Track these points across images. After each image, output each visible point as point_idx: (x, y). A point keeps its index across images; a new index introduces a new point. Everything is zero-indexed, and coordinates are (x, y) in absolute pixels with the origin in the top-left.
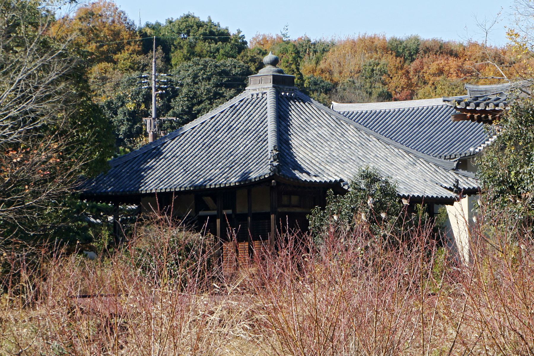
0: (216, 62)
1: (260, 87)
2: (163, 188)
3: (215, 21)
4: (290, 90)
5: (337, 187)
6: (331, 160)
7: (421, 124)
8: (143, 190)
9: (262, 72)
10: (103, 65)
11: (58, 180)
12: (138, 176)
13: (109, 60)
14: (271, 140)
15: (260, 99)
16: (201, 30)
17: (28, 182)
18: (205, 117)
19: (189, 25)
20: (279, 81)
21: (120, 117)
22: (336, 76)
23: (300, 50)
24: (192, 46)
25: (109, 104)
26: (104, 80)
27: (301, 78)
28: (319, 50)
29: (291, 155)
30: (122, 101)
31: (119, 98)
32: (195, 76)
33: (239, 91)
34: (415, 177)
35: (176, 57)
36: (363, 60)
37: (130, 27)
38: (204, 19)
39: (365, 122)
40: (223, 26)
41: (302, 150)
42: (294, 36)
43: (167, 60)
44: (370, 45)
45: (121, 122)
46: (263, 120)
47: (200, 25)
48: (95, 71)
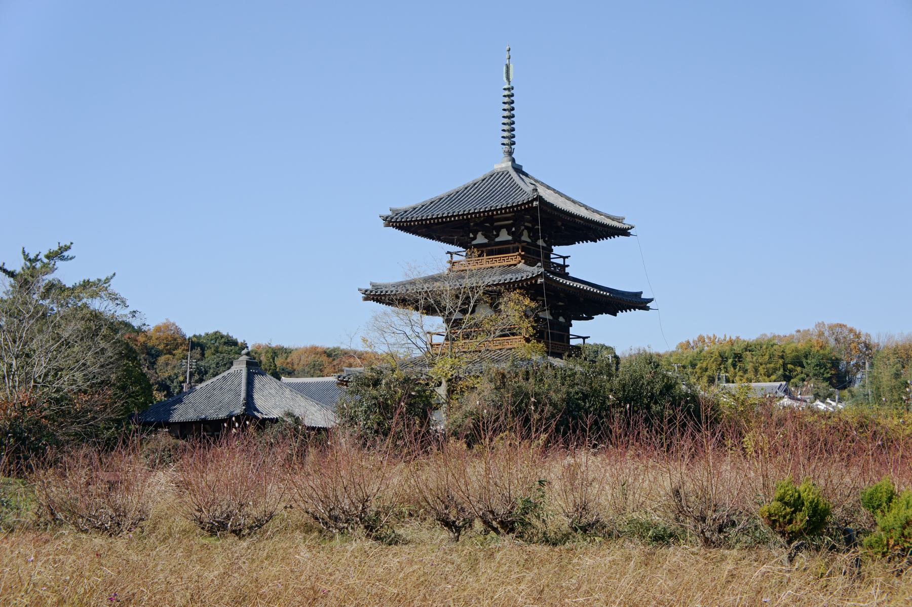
0: (216, 351)
1: (240, 367)
2: (182, 419)
3: (230, 335)
4: (254, 367)
5: (274, 421)
6: (275, 406)
7: (328, 390)
8: (171, 420)
9: (241, 358)
10: (167, 356)
11: (109, 410)
12: (169, 413)
13: (170, 353)
14: (243, 395)
15: (238, 374)
16: (223, 340)
17: (90, 411)
18: (209, 382)
19: (217, 336)
20: (249, 364)
21: (175, 384)
22: (295, 367)
23: (275, 353)
24: (217, 347)
25: (169, 377)
26: (167, 364)
27: (275, 366)
28: (287, 352)
29: (253, 403)
30: (177, 376)
31: (175, 374)
32: (218, 363)
33: (229, 368)
34: (317, 416)
35: (208, 353)
36: (311, 358)
37: (183, 336)
38: (225, 333)
39: (300, 389)
40: (234, 338)
41: (259, 401)
42: (274, 345)
43: (203, 355)
44: (314, 350)
45: (176, 387)
46: (239, 384)
47: (222, 337)
48: (162, 360)
